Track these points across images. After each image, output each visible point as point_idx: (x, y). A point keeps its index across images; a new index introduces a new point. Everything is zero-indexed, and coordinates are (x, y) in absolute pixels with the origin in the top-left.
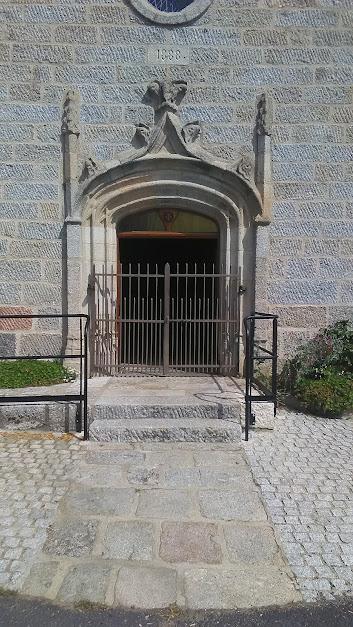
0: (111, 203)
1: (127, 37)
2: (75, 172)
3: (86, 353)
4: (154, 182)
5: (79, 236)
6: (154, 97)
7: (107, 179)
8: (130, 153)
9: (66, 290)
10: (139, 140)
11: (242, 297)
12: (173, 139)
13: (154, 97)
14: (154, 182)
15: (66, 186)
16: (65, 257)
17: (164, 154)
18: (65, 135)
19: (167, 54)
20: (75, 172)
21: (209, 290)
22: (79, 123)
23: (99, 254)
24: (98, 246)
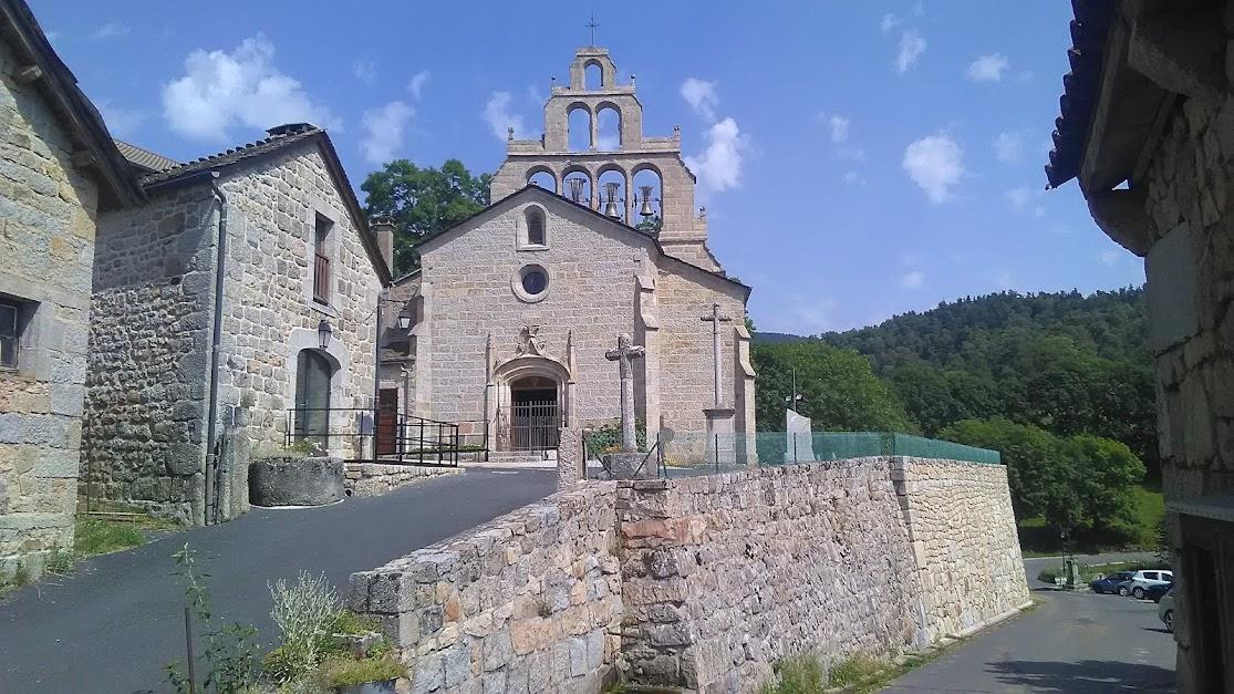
0: (507, 376)
1: (514, 307)
2: (492, 364)
3: (405, 463)
4: (16, 27)
5: (493, 391)
6: (525, 333)
7: (505, 367)
8: (515, 356)
9: (737, 396)
10: (519, 350)
11: (1093, 169)
12: (532, 349)
13: (525, 333)
14: (16, 27)
15: (487, 370)
16: (486, 400)
17: (529, 355)
18: (488, 349)
19: (531, 314)
20: (492, 364)
21: (552, 412)
22: (493, 343)
23: (502, 398)
24: (502, 395)
